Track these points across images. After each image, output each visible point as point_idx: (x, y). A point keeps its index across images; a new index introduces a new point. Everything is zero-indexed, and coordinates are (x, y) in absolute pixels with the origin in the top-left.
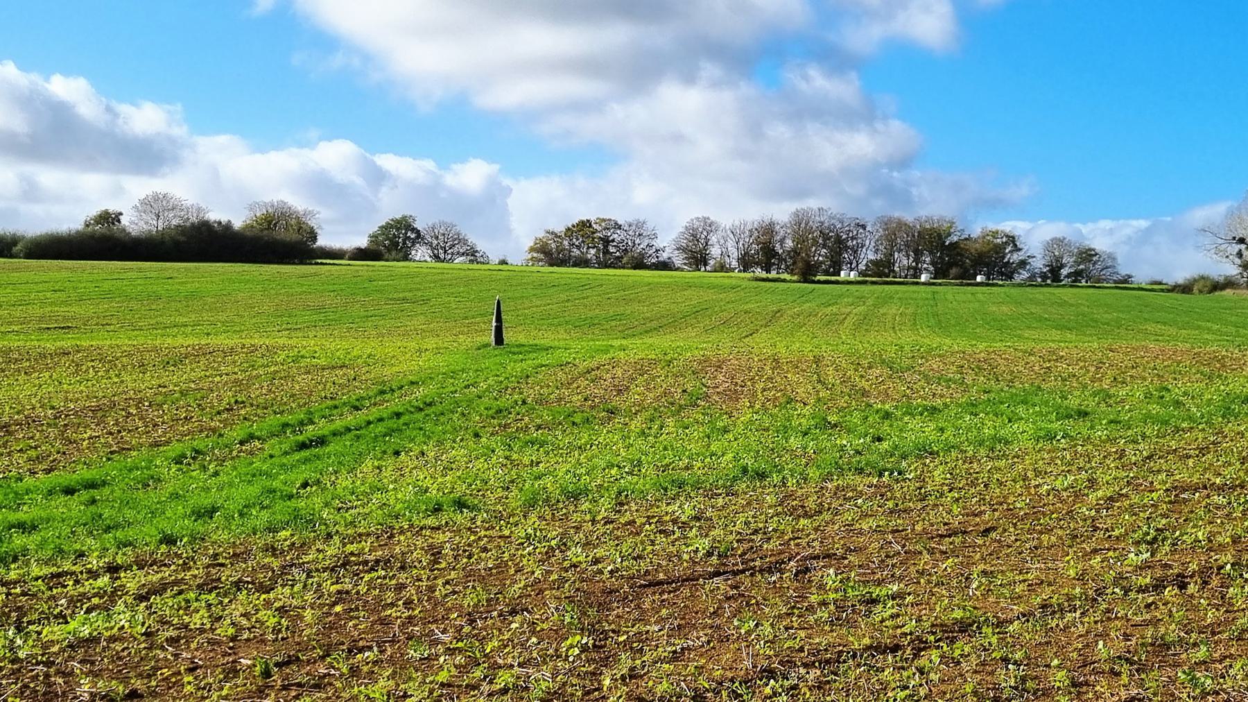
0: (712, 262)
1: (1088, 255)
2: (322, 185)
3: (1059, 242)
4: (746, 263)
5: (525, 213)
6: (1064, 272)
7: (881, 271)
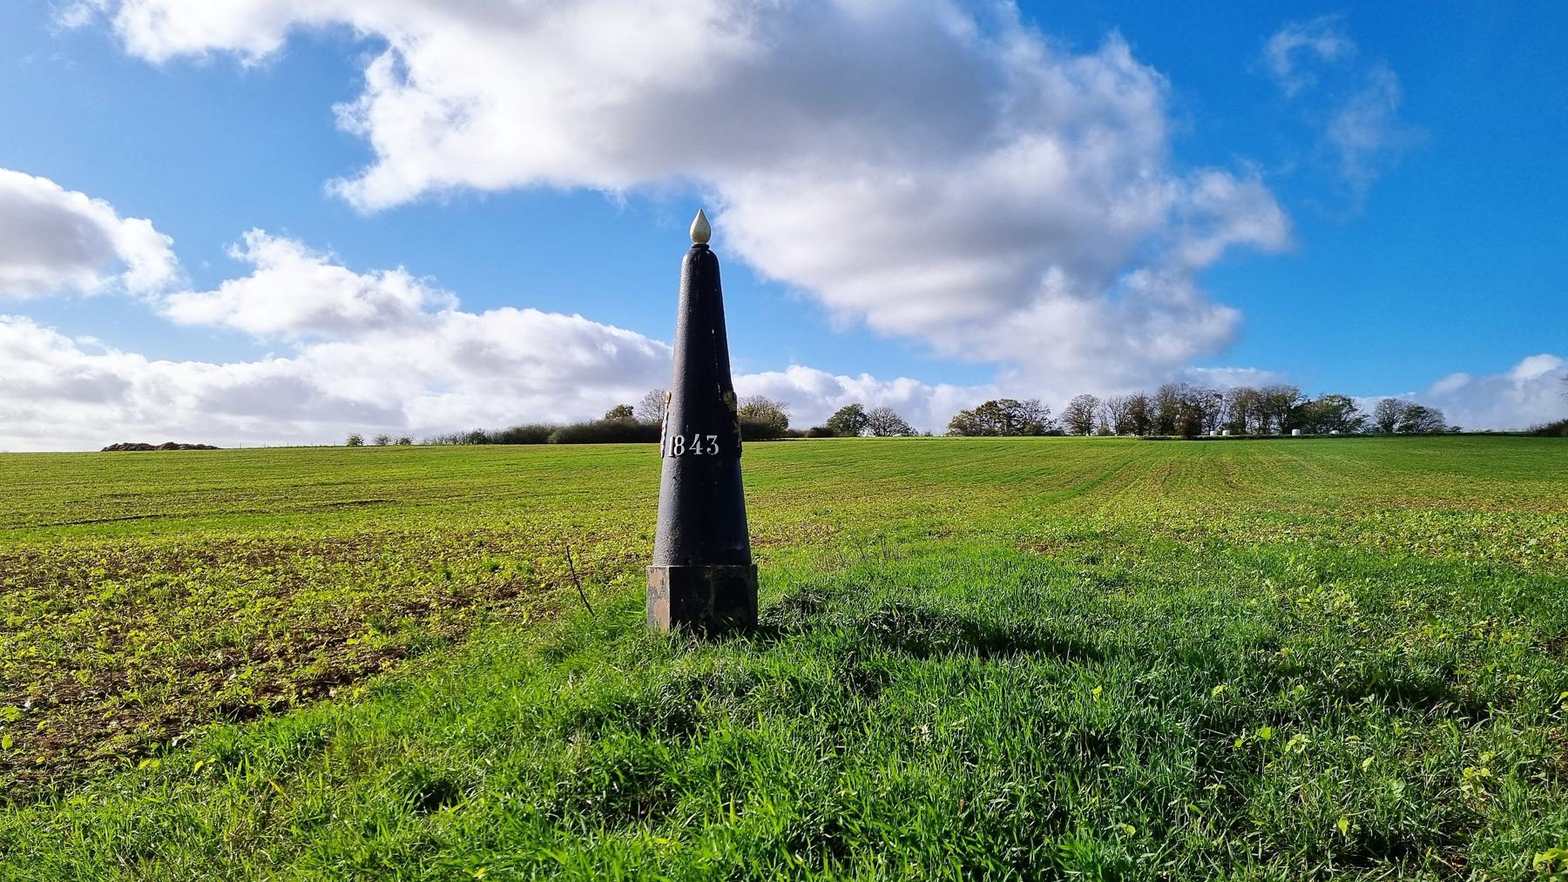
0: (1095, 430)
1: (1418, 412)
2: (798, 397)
3: (1392, 403)
4: (1122, 429)
5: (939, 406)
6: (1396, 426)
7: (1238, 430)
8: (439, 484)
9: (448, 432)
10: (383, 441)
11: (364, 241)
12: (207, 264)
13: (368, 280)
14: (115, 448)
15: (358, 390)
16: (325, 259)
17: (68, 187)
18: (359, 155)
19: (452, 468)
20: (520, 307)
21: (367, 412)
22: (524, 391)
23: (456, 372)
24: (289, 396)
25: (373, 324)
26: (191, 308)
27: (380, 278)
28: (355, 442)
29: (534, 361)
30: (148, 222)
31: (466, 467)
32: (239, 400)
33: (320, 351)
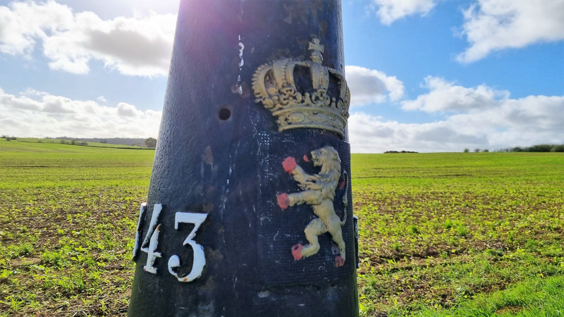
8: (493, 168)
9: (504, 147)
10: (477, 151)
11: (468, 76)
12: (414, 90)
13: (471, 89)
14: (387, 152)
15: (469, 131)
16: (453, 83)
17: (372, 68)
18: (464, 44)
19: (502, 162)
20: (536, 95)
21: (471, 139)
22: (539, 130)
23: (508, 123)
24: (444, 135)
25: (474, 106)
26: (410, 106)
27: (476, 89)
28: (466, 151)
29: (543, 117)
30: (395, 77)
31: (509, 161)
32: (427, 136)
33: (454, 118)
